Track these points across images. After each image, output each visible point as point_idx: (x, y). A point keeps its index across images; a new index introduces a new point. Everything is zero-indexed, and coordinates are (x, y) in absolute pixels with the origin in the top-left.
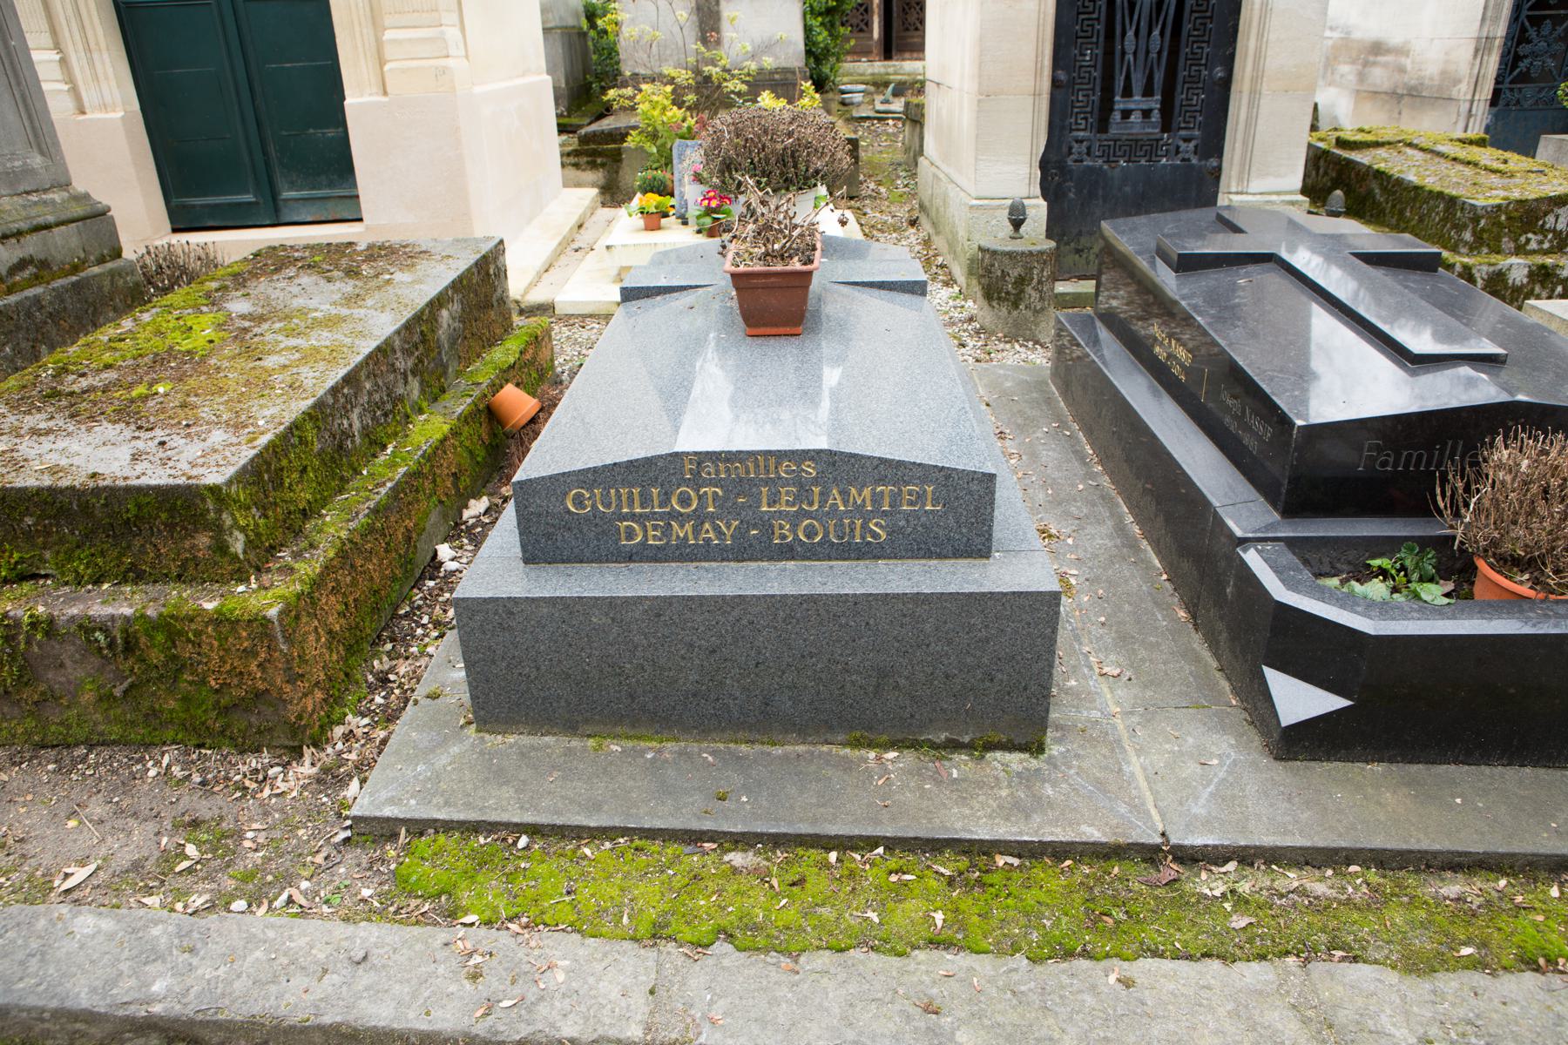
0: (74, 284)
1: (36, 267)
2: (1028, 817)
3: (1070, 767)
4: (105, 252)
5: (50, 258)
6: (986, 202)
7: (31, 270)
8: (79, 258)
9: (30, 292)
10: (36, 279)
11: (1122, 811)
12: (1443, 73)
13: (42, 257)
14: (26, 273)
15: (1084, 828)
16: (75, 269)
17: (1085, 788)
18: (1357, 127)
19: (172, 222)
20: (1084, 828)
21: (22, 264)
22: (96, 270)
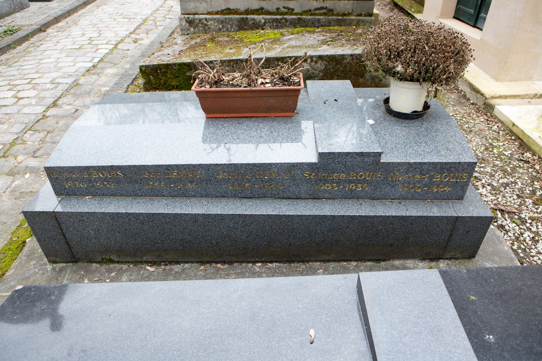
0: (337, 19)
1: (327, 10)
2: (27, 256)
3: (39, 270)
4: (363, 13)
5: (334, 9)
6: (245, 115)
7: (325, 11)
8: (348, 12)
9: (320, 17)
10: (325, 14)
11: (12, 283)
12: (62, 316)
13: (331, 8)
14: (322, 11)
15: (13, 270)
16: (344, 15)
17: (27, 273)
18: (314, 341)
19: (455, 14)
20: (13, 270)
21: (322, 8)
22: (353, 18)
